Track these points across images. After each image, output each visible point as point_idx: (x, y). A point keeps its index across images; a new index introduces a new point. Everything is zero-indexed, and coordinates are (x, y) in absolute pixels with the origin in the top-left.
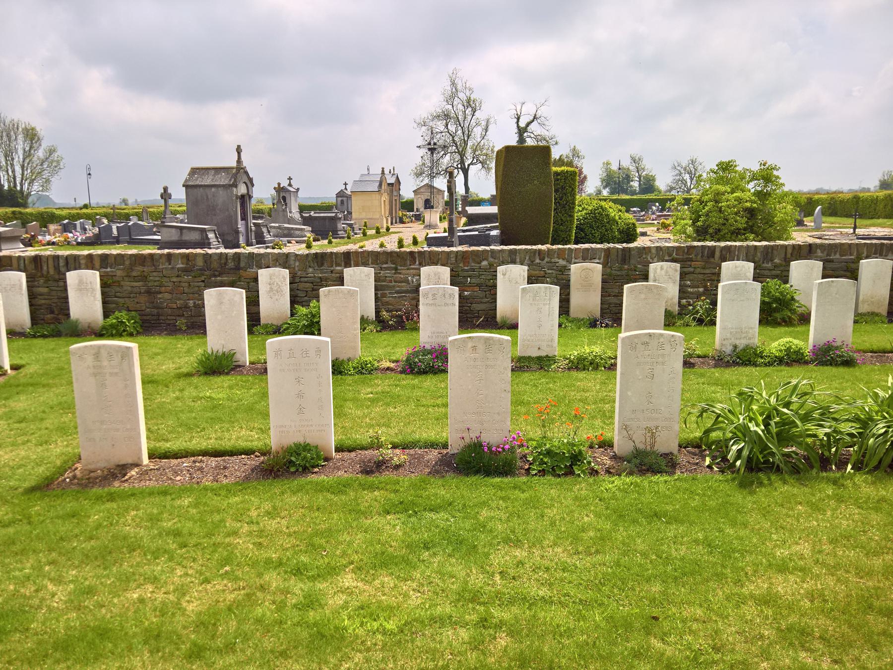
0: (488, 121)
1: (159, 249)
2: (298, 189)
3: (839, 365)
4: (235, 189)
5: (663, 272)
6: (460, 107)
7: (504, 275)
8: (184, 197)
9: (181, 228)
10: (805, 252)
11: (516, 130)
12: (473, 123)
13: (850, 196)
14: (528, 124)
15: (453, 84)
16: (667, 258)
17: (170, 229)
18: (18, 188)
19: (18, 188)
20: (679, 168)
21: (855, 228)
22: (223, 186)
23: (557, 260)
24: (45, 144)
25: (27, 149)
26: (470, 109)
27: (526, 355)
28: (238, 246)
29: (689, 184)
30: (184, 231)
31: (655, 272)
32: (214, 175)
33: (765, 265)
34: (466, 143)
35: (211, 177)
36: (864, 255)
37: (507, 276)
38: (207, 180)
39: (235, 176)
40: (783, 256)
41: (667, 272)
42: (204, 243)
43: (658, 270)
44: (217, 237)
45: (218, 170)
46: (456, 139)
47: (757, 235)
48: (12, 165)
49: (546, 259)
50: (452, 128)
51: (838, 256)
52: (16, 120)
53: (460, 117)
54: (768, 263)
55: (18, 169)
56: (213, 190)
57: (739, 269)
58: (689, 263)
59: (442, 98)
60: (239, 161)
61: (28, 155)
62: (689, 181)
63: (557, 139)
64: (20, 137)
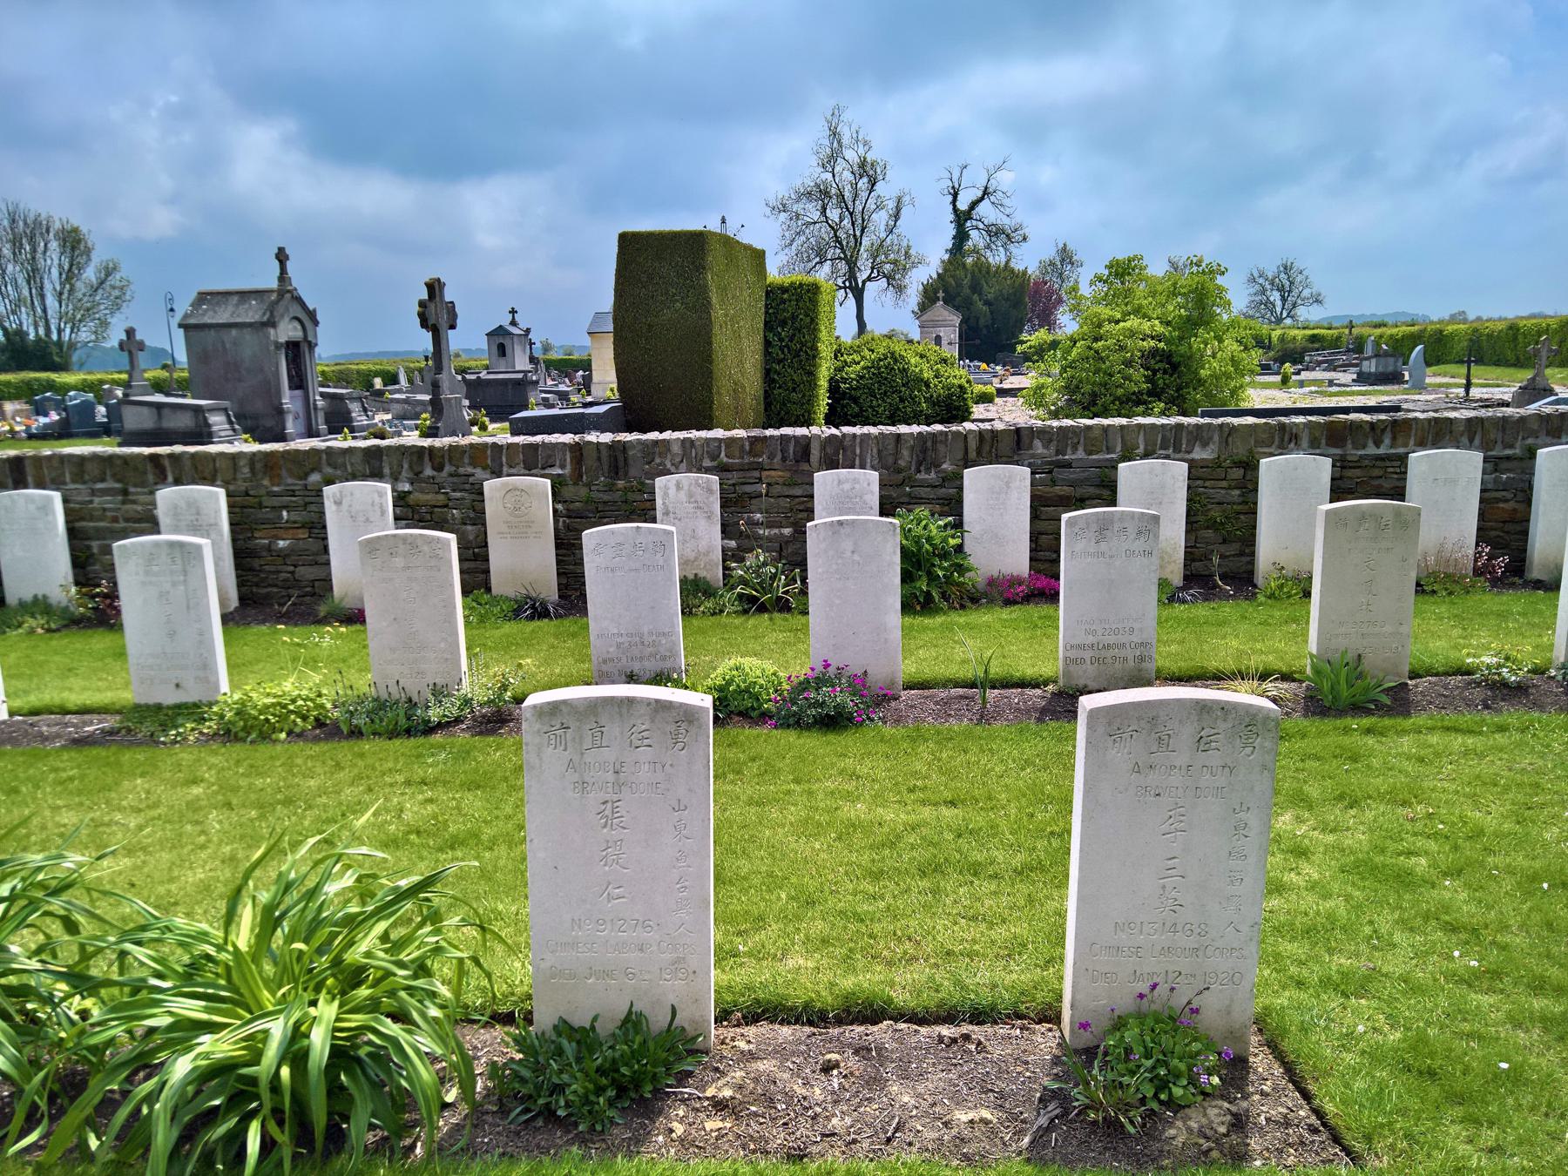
0: (899, 200)
1: (120, 445)
2: (528, 331)
3: (809, 727)
4: (272, 331)
5: (682, 495)
6: (847, 175)
7: (338, 503)
8: (486, 347)
9: (159, 407)
10: (1006, 446)
11: (952, 217)
12: (871, 205)
13: (1501, 326)
14: (974, 205)
15: (834, 134)
16: (707, 463)
17: (139, 408)
18: (55, 337)
19: (55, 337)
20: (1261, 281)
21: (1468, 387)
22: (250, 325)
23: (470, 470)
24: (97, 258)
25: (66, 267)
26: (865, 180)
27: (151, 701)
28: (282, 438)
29: (1278, 309)
30: (166, 411)
31: (666, 494)
32: (237, 306)
33: (922, 476)
34: (858, 242)
35: (230, 308)
36: (1141, 450)
37: (345, 506)
38: (223, 316)
39: (272, 308)
40: (960, 455)
41: (690, 495)
42: (203, 435)
43: (672, 491)
44: (230, 422)
45: (244, 295)
46: (841, 234)
47: (1171, 401)
48: (42, 297)
49: (448, 469)
50: (834, 214)
51: (1080, 454)
52: (43, 216)
53: (847, 194)
54: (928, 471)
55: (51, 301)
56: (234, 332)
57: (847, 486)
58: (756, 474)
59: (814, 161)
60: (283, 277)
61: (69, 276)
62: (1279, 303)
63: (1026, 231)
64: (54, 245)
